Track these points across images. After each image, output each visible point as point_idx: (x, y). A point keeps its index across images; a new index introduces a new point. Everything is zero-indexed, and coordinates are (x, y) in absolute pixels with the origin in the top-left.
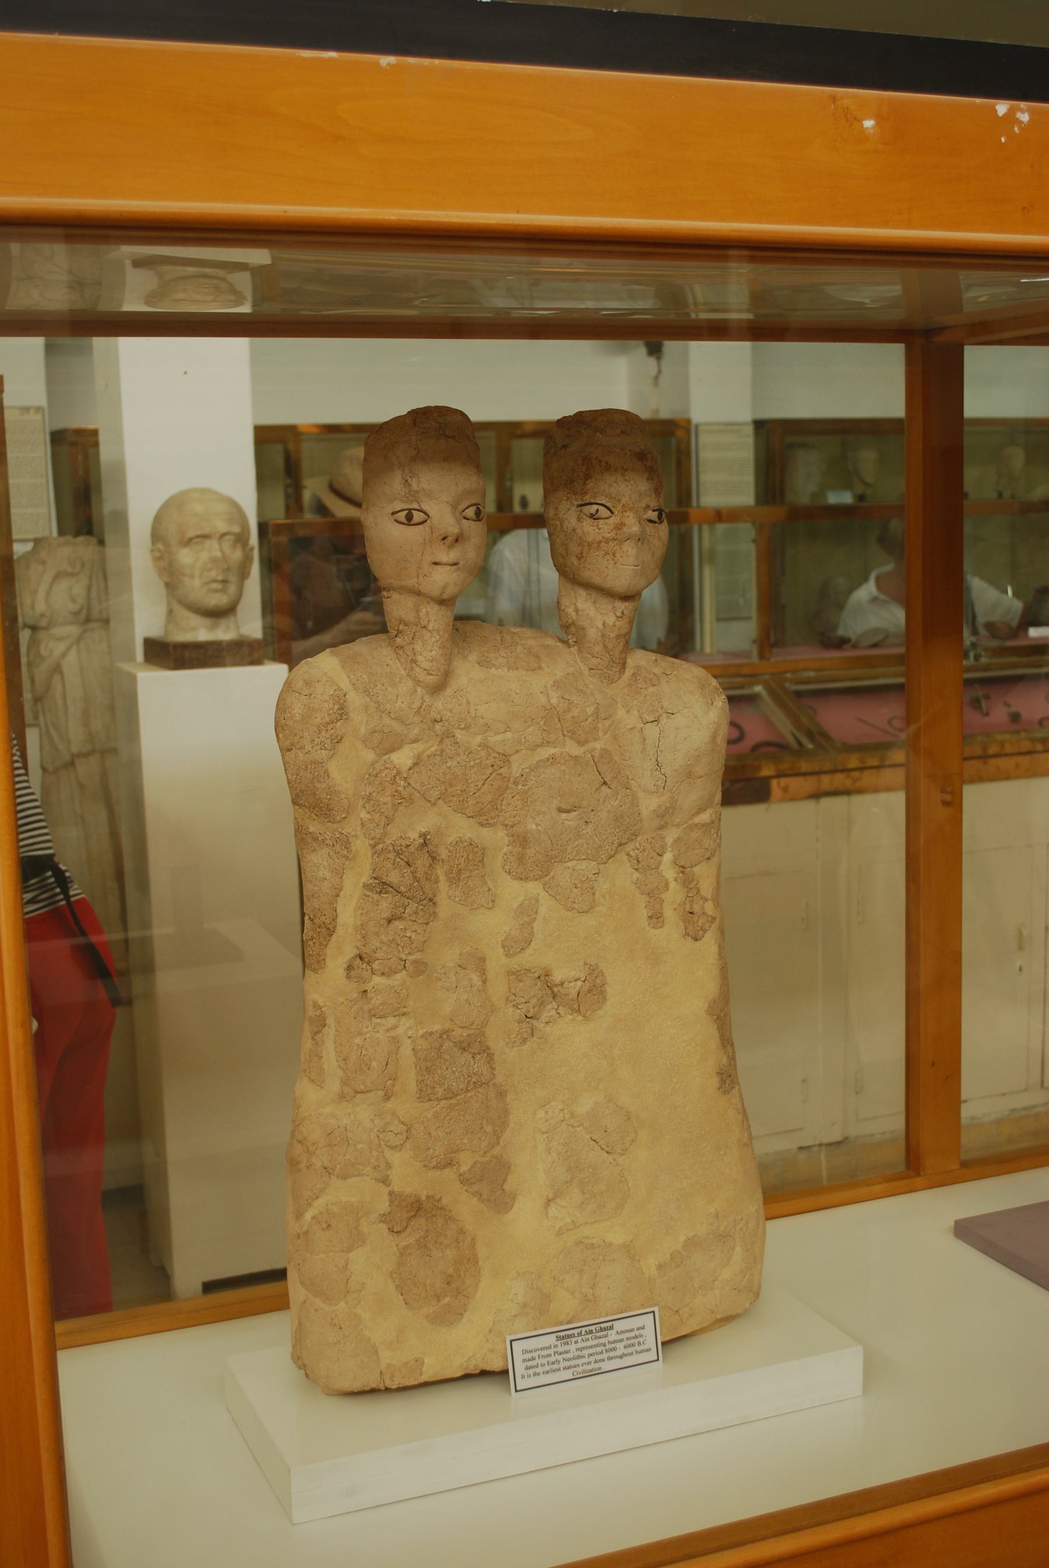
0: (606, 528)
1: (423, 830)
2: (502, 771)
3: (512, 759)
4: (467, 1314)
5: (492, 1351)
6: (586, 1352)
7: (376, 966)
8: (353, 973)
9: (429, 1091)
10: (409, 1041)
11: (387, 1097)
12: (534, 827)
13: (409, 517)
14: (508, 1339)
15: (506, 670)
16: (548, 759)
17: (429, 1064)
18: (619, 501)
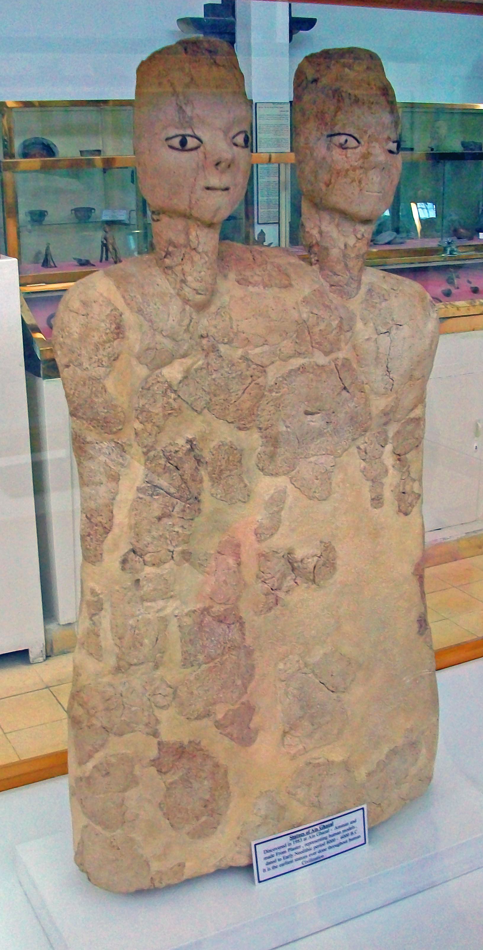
0: (353, 156)
1: (190, 437)
2: (259, 380)
3: (268, 369)
4: (220, 827)
5: (239, 853)
6: (312, 846)
7: (147, 558)
8: (128, 566)
9: (192, 659)
10: (175, 619)
11: (156, 667)
12: (284, 429)
13: (183, 143)
14: (253, 844)
15: (261, 287)
16: (299, 369)
17: (192, 637)
18: (366, 132)
